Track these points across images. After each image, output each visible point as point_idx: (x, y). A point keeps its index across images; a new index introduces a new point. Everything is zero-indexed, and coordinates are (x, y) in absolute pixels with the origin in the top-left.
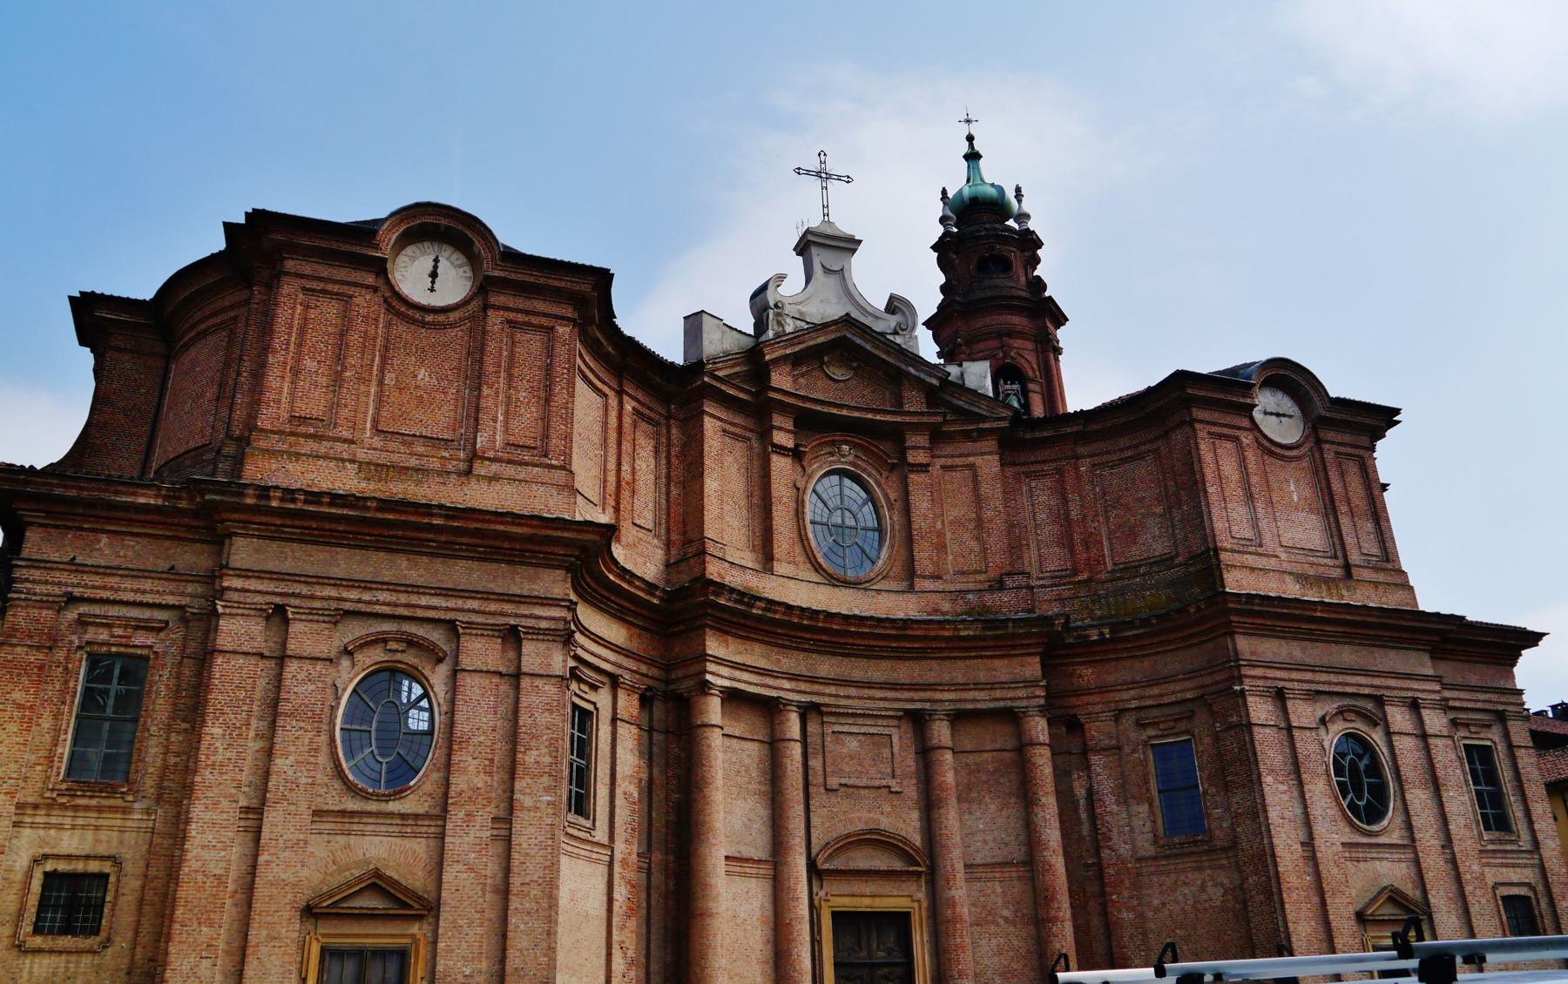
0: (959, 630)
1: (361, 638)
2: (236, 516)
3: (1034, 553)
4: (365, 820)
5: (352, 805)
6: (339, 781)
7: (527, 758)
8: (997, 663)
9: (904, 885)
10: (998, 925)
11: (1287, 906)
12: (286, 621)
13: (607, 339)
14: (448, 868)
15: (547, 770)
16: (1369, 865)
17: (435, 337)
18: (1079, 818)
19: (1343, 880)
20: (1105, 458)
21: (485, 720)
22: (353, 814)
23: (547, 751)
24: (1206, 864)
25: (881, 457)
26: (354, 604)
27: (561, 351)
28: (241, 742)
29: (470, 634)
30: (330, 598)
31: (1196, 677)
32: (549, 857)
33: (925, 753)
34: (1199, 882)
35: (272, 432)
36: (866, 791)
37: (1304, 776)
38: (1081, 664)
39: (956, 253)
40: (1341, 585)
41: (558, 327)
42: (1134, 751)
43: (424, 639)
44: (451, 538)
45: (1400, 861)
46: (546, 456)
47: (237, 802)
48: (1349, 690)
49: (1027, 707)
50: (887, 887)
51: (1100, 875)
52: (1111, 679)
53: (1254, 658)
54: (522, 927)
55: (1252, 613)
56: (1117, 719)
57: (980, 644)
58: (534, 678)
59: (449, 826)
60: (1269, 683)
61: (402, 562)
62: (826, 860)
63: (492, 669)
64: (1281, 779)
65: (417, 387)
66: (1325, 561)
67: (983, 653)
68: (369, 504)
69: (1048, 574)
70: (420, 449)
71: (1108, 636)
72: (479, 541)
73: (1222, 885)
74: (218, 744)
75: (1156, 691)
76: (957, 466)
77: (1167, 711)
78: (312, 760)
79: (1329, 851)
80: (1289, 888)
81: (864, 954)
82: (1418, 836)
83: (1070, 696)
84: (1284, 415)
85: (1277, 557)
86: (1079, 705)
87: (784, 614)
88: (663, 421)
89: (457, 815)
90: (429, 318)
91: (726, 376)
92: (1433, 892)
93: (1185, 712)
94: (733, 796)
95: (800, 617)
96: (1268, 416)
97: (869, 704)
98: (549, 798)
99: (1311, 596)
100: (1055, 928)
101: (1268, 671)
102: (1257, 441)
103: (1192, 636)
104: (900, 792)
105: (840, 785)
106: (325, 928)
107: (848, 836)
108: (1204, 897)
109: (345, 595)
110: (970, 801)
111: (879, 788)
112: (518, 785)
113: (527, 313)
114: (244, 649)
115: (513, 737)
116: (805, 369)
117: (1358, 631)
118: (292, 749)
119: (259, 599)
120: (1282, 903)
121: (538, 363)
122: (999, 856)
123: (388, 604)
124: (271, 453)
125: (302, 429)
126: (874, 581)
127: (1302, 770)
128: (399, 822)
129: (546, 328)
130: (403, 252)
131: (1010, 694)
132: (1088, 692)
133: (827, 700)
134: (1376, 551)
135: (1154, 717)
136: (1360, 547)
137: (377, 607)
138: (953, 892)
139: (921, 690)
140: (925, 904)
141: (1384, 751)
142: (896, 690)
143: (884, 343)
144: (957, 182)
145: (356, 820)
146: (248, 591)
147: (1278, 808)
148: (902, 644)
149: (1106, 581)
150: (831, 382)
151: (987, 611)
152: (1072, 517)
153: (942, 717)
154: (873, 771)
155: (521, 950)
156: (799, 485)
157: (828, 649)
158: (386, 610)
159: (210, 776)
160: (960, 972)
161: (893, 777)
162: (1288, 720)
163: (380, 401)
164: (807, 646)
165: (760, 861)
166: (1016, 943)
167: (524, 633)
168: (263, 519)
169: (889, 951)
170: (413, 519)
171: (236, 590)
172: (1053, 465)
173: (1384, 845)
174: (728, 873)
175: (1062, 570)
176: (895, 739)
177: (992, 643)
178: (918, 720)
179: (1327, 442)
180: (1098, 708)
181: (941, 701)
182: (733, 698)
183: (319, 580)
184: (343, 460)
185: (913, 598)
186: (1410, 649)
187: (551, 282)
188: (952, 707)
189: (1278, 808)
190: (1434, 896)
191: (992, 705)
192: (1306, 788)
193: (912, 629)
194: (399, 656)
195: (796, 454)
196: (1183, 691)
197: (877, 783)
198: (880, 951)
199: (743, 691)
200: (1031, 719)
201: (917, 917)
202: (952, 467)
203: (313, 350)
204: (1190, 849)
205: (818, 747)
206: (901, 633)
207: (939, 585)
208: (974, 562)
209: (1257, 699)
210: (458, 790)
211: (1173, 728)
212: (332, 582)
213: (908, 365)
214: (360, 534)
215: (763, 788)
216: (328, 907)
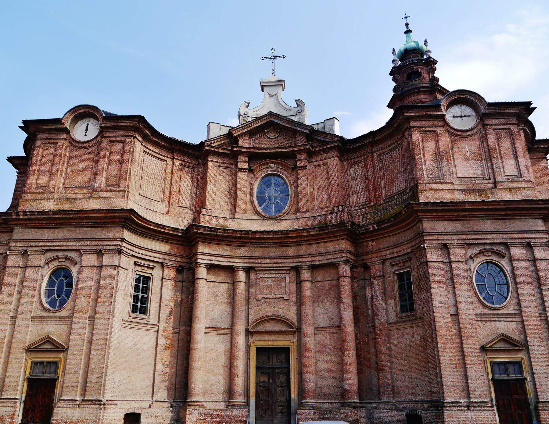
0: (310, 232)
1: (50, 258)
2: (13, 223)
4: (48, 319)
5: (45, 314)
7: (102, 295)
8: (329, 244)
9: (287, 337)
10: (327, 352)
11: (439, 344)
13: (161, 140)
15: (108, 299)
16: (493, 324)
17: (86, 151)
18: (367, 307)
20: (384, 151)
21: (88, 283)
22: (44, 317)
24: (414, 325)
25: (287, 166)
27: (441, 138)
28: (12, 296)
30: (41, 246)
31: (410, 242)
33: (299, 282)
34: (412, 333)
35: (29, 193)
37: (456, 284)
39: (398, 74)
40: (488, 192)
42: (390, 277)
44: (80, 221)
45: (512, 321)
47: (9, 315)
48: (488, 241)
50: (280, 337)
51: (374, 331)
52: (381, 246)
53: (433, 231)
54: (95, 354)
55: (429, 211)
59: (74, 320)
60: (440, 242)
61: (66, 231)
62: (254, 327)
64: (442, 286)
65: (78, 170)
67: (323, 241)
69: (360, 204)
70: (77, 191)
71: (376, 228)
72: (89, 221)
73: (420, 334)
74: (5, 297)
75: (397, 250)
76: (321, 165)
77: (402, 258)
78: (32, 300)
79: (467, 318)
80: (441, 336)
81: (270, 363)
82: (524, 309)
83: (365, 255)
84: (465, 116)
85: (452, 183)
86: (368, 259)
87: (233, 233)
88: (196, 166)
89: (77, 316)
90: (83, 145)
92: (530, 336)
93: (408, 258)
96: (456, 118)
99: (470, 199)
101: (440, 236)
102: (448, 131)
103: (409, 224)
104: (288, 300)
105: (262, 298)
106: (33, 355)
107: (262, 318)
108: (414, 340)
109: (46, 244)
111: (279, 298)
112: (98, 305)
113: (116, 137)
114: (15, 265)
115: (98, 289)
116: (258, 136)
117: (494, 213)
118: (27, 297)
119: (20, 249)
120: (437, 342)
121: (119, 154)
122: (329, 323)
123: (60, 246)
124: (27, 200)
125: (39, 191)
129: (123, 141)
131: (333, 257)
132: (372, 253)
133: (256, 265)
134: (515, 172)
135: (396, 262)
136: (505, 172)
138: (306, 339)
139: (297, 258)
140: (296, 344)
141: (508, 270)
142: (287, 259)
143: (286, 120)
144: (401, 44)
146: (17, 246)
147: (439, 299)
148: (288, 240)
151: (326, 223)
152: (369, 178)
153: (305, 268)
154: (277, 292)
156: (252, 182)
157: (258, 245)
158: (59, 248)
159: (2, 307)
160: (307, 372)
161: (286, 294)
162: (449, 258)
164: (248, 245)
165: (224, 328)
166: (334, 359)
168: (21, 222)
169: (281, 362)
170: (64, 216)
171: (13, 247)
174: (206, 333)
176: (287, 278)
177: (325, 236)
178: (297, 270)
179: (488, 125)
180: (376, 259)
181: (305, 262)
182: (211, 267)
183: (38, 240)
185: (296, 221)
186: (529, 219)
187: (122, 124)
188: (310, 264)
189: (439, 299)
190: (531, 338)
191: (326, 262)
192: (457, 289)
193: (290, 234)
194: (63, 263)
195: (250, 171)
196: (407, 249)
197: (278, 296)
200: (341, 266)
202: (319, 165)
205: (254, 284)
206: (286, 236)
207: (307, 215)
209: (433, 250)
213: (297, 127)
215: (229, 301)
216: (490, 347)
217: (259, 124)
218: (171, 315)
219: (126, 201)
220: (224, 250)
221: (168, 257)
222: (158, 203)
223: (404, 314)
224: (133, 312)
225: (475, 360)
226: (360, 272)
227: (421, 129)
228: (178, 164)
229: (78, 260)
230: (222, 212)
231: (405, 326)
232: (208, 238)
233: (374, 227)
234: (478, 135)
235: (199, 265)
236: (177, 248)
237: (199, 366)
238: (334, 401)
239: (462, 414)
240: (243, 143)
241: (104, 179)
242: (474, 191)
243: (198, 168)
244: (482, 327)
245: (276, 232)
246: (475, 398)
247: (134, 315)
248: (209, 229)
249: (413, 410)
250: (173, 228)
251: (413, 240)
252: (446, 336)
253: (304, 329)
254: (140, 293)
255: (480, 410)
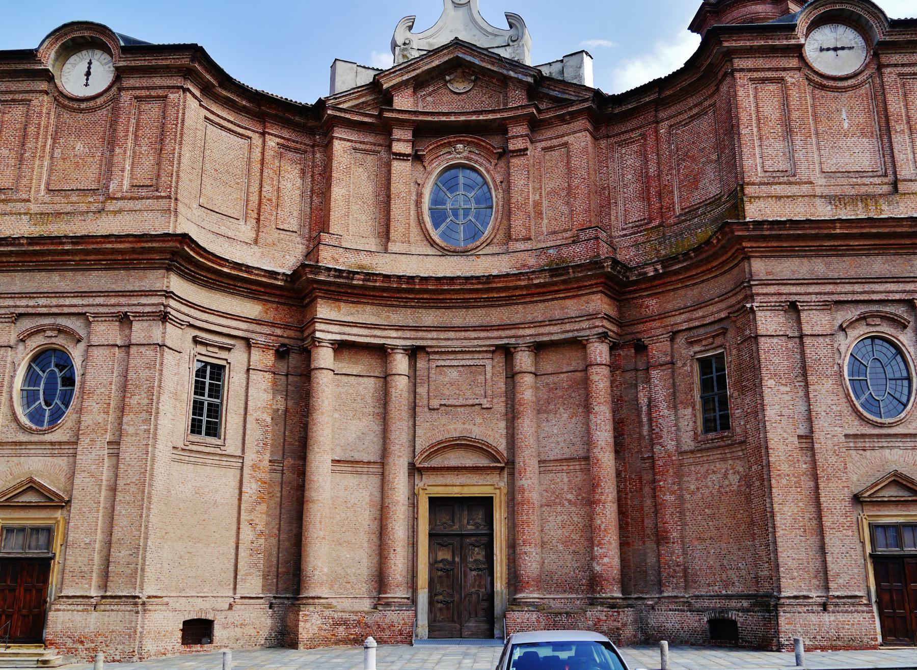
0: (532, 279)
3: (621, 208)
6: (15, 423)
7: (132, 401)
8: (569, 302)
9: (488, 477)
10: (563, 506)
11: (774, 490)
12: (798, 312)
13: (238, 96)
14: (78, 476)
15: (145, 408)
16: (877, 453)
17: (88, 118)
19: (841, 467)
22: (21, 443)
23: (146, 395)
24: (729, 455)
25: (489, 149)
26: (25, 309)
29: (97, 321)
30: (9, 307)
32: (144, 466)
33: (512, 376)
36: (463, 408)
37: (810, 378)
38: (648, 296)
41: (170, 95)
42: (684, 365)
43: (66, 327)
44: (83, 257)
46: (157, 191)
49: (588, 336)
50: (474, 479)
51: (653, 467)
52: (669, 306)
54: (124, 512)
56: (672, 339)
57: (552, 289)
58: (139, 347)
59: (80, 448)
60: (783, 298)
61: (56, 277)
63: (111, 343)
64: (784, 382)
65: (75, 156)
66: (871, 180)
67: (557, 296)
68: (22, 241)
69: (630, 225)
71: (661, 271)
72: (101, 257)
73: (739, 473)
75: (700, 313)
76: (555, 146)
77: (709, 329)
80: (779, 475)
81: (457, 527)
83: (638, 324)
84: (843, 48)
85: (811, 183)
87: (383, 281)
88: (309, 149)
89: (85, 441)
90: (83, 106)
91: (353, 107)
93: (721, 328)
94: (349, 418)
95: (398, 283)
96: (824, 52)
97: (466, 343)
98: (145, 427)
99: (846, 214)
100: (598, 508)
103: (724, 263)
104: (491, 408)
105: (441, 405)
108: (727, 483)
109: (18, 303)
110: (546, 412)
111: (473, 405)
113: (148, 88)
116: (431, 89)
117: (891, 242)
120: (771, 488)
126: (479, 248)
127: (809, 373)
128: (50, 447)
130: (68, 62)
131: (577, 326)
132: (651, 319)
133: (429, 343)
137: (39, 309)
138: (523, 482)
140: (505, 491)
142: (488, 330)
145: (24, 447)
147: (777, 407)
148: (491, 295)
149: (675, 224)
150: (454, 96)
151: (563, 262)
153: (523, 349)
155: (122, 527)
157: (432, 305)
158: (44, 310)
161: (485, 397)
163: (51, 170)
164: (413, 304)
165: (369, 463)
167: (757, 307)
169: (477, 526)
170: (51, 247)
172: (638, 132)
173: (896, 435)
175: (641, 220)
178: (507, 352)
179: (889, 66)
180: (659, 331)
181: (523, 336)
182: (341, 347)
184: (20, 214)
187: (160, 63)
189: (777, 407)
192: (811, 388)
193: (495, 282)
194: (53, 340)
195: (417, 158)
196: (718, 312)
197: (471, 402)
198: (467, 524)
199: (354, 342)
200: (591, 345)
201: (498, 500)
202: (551, 147)
203: (6, 142)
204: (719, 444)
206: (486, 286)
207: (528, 245)
208: (563, 223)
209: (768, 313)
210: (86, 424)
211: (712, 343)
212: (9, 296)
214: (26, 262)
215: (377, 411)
216: (870, 496)
217: (434, 64)
218: (267, 438)
219: (172, 218)
220: (367, 314)
221: (258, 328)
222: (236, 221)
223: (711, 436)
224: (193, 432)
225: (841, 520)
226: (627, 355)
227: (756, 75)
228: (274, 144)
229: (82, 333)
230: (363, 240)
231: (711, 458)
232: (334, 291)
233: (656, 270)
234: (867, 86)
235: (319, 342)
236: (276, 309)
237: (322, 533)
238: (574, 596)
239: (813, 618)
240: (403, 102)
241: (127, 174)
242: (854, 199)
243: (314, 153)
244: (856, 458)
245: (438, 279)
246: (837, 590)
247: (195, 438)
248: (337, 274)
249: (722, 612)
250: (266, 271)
251: (731, 294)
252: (788, 475)
253: (519, 463)
254: (206, 397)
255: (847, 612)
